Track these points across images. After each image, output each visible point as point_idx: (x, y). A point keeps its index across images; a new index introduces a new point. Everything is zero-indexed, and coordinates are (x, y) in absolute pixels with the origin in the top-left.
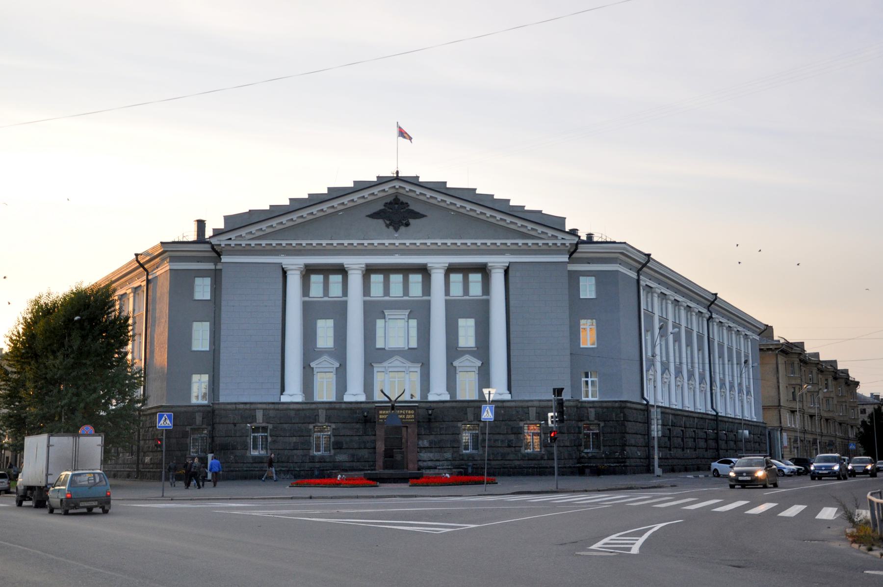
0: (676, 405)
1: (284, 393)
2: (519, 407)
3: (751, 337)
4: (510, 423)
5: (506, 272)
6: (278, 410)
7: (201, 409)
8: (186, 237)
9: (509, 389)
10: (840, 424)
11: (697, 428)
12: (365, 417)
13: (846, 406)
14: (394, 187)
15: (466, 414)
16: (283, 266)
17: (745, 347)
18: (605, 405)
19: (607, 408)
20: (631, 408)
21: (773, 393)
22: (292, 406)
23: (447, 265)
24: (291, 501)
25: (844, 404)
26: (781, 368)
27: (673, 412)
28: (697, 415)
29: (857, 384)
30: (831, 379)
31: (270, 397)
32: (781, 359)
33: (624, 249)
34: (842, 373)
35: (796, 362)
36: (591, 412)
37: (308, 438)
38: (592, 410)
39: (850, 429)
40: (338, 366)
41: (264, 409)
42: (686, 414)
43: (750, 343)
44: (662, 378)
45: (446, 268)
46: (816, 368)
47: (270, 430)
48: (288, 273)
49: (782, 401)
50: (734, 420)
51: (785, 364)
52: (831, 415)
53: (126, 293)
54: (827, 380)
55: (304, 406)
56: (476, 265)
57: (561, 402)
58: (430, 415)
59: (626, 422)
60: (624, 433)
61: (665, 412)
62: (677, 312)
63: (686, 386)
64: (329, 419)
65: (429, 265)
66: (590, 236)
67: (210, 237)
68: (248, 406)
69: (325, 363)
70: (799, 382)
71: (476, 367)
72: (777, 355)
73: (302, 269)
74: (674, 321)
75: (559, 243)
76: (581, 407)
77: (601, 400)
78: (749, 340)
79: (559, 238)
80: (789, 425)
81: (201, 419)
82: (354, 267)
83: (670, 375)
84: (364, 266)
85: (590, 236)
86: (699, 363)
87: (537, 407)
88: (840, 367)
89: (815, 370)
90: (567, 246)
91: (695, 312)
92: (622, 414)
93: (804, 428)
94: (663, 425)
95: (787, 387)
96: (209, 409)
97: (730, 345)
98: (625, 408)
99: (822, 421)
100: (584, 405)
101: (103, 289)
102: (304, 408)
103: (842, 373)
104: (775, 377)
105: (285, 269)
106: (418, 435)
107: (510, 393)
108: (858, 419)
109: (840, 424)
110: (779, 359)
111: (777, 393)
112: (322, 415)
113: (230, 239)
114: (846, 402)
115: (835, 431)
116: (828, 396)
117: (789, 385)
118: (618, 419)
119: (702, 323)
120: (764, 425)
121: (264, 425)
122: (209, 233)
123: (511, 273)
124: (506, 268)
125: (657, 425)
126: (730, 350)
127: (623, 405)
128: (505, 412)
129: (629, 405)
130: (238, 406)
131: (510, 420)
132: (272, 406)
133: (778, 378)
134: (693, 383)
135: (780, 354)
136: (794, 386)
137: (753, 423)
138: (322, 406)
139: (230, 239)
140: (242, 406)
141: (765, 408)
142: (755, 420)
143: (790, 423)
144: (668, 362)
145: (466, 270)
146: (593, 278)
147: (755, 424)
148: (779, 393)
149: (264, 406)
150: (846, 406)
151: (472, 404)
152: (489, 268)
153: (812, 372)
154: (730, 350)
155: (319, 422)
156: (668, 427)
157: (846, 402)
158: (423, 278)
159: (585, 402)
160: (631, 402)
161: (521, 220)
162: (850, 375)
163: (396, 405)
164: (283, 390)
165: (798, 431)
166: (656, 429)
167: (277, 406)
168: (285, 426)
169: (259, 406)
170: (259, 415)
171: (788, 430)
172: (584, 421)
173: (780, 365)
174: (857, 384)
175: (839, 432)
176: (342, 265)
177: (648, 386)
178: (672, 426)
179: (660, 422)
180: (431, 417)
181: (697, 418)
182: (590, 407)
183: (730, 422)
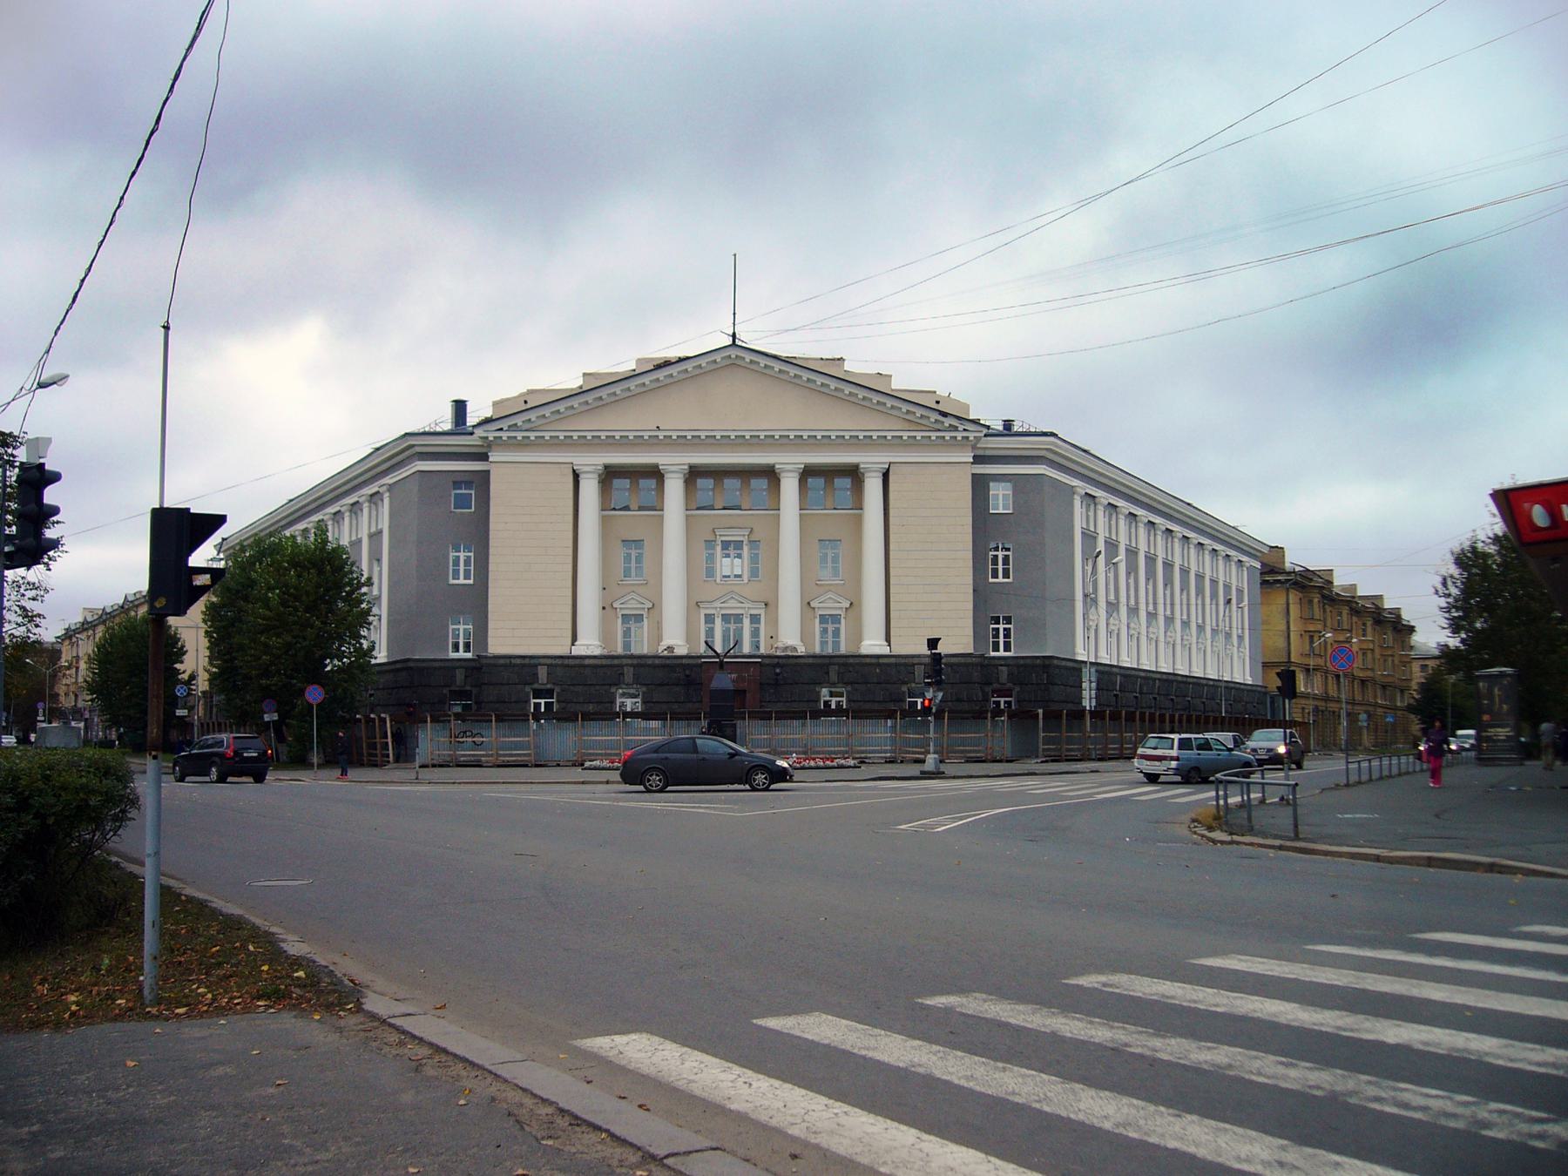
0: (1127, 662)
1: (576, 643)
2: (900, 665)
3: (1248, 565)
4: (889, 686)
5: (886, 476)
6: (568, 666)
7: (463, 664)
8: (441, 425)
9: (888, 639)
10: (1384, 687)
11: (1158, 694)
12: (687, 676)
13: (1393, 661)
14: (730, 356)
15: (827, 673)
16: (575, 468)
17: (1239, 578)
18: (1022, 662)
19: (1025, 666)
20: (1058, 667)
21: (1281, 643)
22: (587, 662)
23: (803, 466)
24: (581, 786)
25: (1390, 659)
26: (1295, 611)
27: (1122, 671)
28: (1158, 676)
29: (1411, 629)
30: (1370, 622)
31: (559, 648)
32: (1294, 597)
33: (1052, 443)
34: (1390, 613)
35: (1316, 600)
36: (1002, 671)
37: (609, 705)
38: (1004, 668)
39: (1399, 695)
40: (848, 606)
41: (548, 665)
42: (1142, 674)
43: (1245, 573)
44: (1107, 624)
45: (801, 471)
46: (1347, 608)
47: (558, 693)
48: (581, 476)
49: (1292, 655)
50: (1189, 680)
51: (1301, 604)
52: (1369, 674)
53: (358, 502)
54: (1364, 624)
55: (604, 662)
56: (849, 466)
57: (938, 656)
58: (778, 674)
59: (1051, 686)
60: (1047, 701)
61: (1106, 674)
62: (1133, 530)
63: (1162, 638)
64: (637, 680)
65: (777, 466)
66: (1008, 424)
67: (474, 426)
68: (527, 661)
69: (733, 601)
70: (1319, 627)
71: (842, 608)
72: (1288, 589)
73: (600, 472)
74: (1147, 550)
75: (959, 435)
76: (988, 665)
77: (1016, 655)
78: (1245, 569)
79: (959, 429)
80: (1303, 689)
81: (463, 677)
82: (673, 468)
83: (1140, 624)
84: (686, 467)
85: (1008, 424)
86: (1165, 604)
87: (925, 665)
88: (1387, 605)
89: (1345, 611)
90: (971, 441)
91: (1078, 494)
92: (1045, 675)
93: (1326, 693)
94: (1098, 689)
95: (1301, 635)
96: (473, 664)
97: (1215, 576)
98: (1049, 665)
99: (1356, 683)
100: (993, 662)
101: (223, 916)
102: (604, 663)
103: (1390, 613)
104: (1285, 622)
105: (577, 472)
106: (761, 702)
107: (889, 645)
108: (1411, 680)
109: (1384, 687)
110: (1291, 596)
111: (1286, 644)
112: (629, 674)
113: (501, 429)
114: (1392, 656)
115: (1375, 697)
116: (1366, 647)
117: (1306, 631)
118: (1039, 682)
119: (1172, 545)
120: (1263, 690)
121: (549, 686)
122: (471, 420)
123: (892, 478)
124: (885, 471)
125: (1090, 690)
126: (1214, 582)
127: (1047, 662)
128: (881, 671)
129: (1055, 662)
130: (513, 661)
131: (888, 683)
132: (559, 662)
133: (1288, 622)
134: (1173, 634)
135: (1293, 588)
136: (1311, 634)
137: (1245, 687)
138: (629, 661)
139: (501, 429)
140: (518, 661)
141: (1266, 665)
142: (1250, 683)
143: (1306, 686)
144: (1118, 602)
145: (829, 473)
146: (1009, 485)
147: (1249, 688)
148: (1289, 644)
149: (549, 661)
150: (1393, 661)
151: (836, 660)
152: (862, 470)
153: (1341, 612)
154: (1214, 582)
155: (624, 684)
156: (1115, 692)
157: (1392, 656)
158: (769, 482)
159: (994, 658)
160: (1058, 658)
161: (906, 403)
162: (1403, 617)
163: (725, 660)
164: (574, 639)
165: (1344, 700)
166: (1088, 697)
167: (566, 662)
168: (579, 689)
169: (542, 661)
170: (542, 673)
171: (1302, 697)
172: (991, 684)
173: (1291, 606)
174: (1411, 629)
175: (1381, 699)
176: (656, 466)
177: (1109, 639)
178: (1120, 691)
179: (1094, 685)
180: (779, 677)
181: (1159, 679)
182: (1001, 665)
183: (1210, 685)
